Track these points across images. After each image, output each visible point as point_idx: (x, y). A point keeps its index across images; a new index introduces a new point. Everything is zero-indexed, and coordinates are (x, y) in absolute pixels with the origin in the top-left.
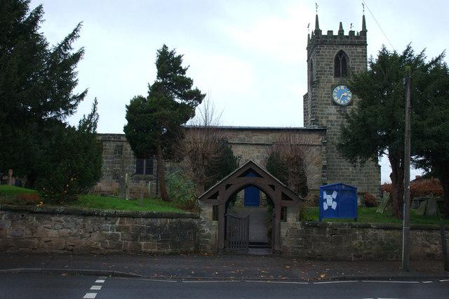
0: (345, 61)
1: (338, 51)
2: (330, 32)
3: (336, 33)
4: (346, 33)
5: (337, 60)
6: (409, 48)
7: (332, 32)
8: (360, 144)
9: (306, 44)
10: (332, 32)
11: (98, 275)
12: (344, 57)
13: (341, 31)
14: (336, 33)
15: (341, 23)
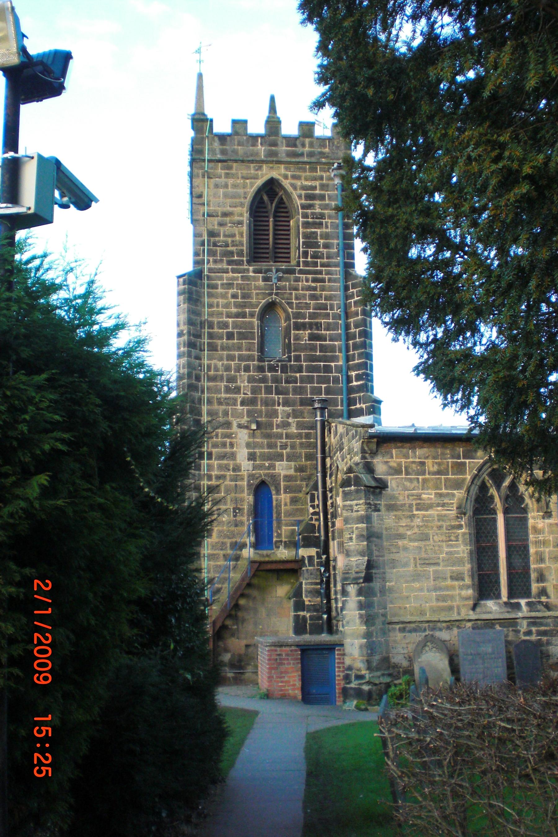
0: (283, 210)
1: (259, 182)
2: (239, 125)
3: (256, 127)
4: (289, 128)
5: (257, 208)
6: (144, 340)
7: (244, 123)
8: (320, 15)
9: (62, 162)
10: (244, 123)
11: (449, 45)
12: (281, 201)
13: (273, 124)
14: (256, 127)
15: (272, 99)
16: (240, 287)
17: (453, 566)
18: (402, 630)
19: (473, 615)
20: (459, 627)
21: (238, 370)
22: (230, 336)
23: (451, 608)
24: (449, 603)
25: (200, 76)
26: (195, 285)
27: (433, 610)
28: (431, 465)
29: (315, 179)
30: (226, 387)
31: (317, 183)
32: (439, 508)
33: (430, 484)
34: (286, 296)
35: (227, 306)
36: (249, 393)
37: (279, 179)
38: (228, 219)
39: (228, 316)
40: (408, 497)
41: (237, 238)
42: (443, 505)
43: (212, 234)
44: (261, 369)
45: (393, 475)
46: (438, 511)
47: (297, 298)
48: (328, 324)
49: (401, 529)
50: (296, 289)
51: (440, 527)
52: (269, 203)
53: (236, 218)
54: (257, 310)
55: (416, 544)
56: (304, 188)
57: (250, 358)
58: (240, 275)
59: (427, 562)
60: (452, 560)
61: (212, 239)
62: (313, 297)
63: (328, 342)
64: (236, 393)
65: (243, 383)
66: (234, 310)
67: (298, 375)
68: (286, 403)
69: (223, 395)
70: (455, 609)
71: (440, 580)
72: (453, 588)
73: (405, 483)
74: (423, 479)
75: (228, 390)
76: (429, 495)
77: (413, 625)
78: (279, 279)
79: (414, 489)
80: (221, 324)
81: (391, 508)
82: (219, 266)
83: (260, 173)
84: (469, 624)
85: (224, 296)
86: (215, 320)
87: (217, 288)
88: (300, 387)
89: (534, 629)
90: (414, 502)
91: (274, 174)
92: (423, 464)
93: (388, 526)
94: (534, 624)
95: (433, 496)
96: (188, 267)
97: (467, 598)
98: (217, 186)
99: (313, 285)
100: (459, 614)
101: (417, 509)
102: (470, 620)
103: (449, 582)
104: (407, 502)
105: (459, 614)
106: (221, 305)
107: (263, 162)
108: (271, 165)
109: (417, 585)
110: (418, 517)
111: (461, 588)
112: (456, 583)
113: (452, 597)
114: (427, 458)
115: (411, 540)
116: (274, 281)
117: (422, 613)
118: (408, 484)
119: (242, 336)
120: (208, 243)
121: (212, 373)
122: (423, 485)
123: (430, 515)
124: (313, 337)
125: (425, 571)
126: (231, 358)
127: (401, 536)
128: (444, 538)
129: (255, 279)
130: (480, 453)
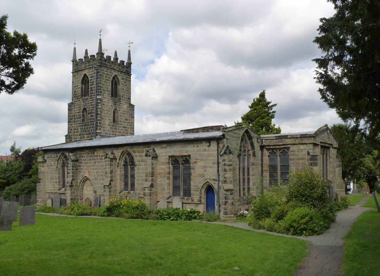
15: (86, 50)
23: (55, 190)
28: (53, 156)
33: (53, 160)
39: (77, 113)
43: (75, 92)
66: (78, 111)
76: (52, 163)
92: (52, 156)
126: (77, 124)
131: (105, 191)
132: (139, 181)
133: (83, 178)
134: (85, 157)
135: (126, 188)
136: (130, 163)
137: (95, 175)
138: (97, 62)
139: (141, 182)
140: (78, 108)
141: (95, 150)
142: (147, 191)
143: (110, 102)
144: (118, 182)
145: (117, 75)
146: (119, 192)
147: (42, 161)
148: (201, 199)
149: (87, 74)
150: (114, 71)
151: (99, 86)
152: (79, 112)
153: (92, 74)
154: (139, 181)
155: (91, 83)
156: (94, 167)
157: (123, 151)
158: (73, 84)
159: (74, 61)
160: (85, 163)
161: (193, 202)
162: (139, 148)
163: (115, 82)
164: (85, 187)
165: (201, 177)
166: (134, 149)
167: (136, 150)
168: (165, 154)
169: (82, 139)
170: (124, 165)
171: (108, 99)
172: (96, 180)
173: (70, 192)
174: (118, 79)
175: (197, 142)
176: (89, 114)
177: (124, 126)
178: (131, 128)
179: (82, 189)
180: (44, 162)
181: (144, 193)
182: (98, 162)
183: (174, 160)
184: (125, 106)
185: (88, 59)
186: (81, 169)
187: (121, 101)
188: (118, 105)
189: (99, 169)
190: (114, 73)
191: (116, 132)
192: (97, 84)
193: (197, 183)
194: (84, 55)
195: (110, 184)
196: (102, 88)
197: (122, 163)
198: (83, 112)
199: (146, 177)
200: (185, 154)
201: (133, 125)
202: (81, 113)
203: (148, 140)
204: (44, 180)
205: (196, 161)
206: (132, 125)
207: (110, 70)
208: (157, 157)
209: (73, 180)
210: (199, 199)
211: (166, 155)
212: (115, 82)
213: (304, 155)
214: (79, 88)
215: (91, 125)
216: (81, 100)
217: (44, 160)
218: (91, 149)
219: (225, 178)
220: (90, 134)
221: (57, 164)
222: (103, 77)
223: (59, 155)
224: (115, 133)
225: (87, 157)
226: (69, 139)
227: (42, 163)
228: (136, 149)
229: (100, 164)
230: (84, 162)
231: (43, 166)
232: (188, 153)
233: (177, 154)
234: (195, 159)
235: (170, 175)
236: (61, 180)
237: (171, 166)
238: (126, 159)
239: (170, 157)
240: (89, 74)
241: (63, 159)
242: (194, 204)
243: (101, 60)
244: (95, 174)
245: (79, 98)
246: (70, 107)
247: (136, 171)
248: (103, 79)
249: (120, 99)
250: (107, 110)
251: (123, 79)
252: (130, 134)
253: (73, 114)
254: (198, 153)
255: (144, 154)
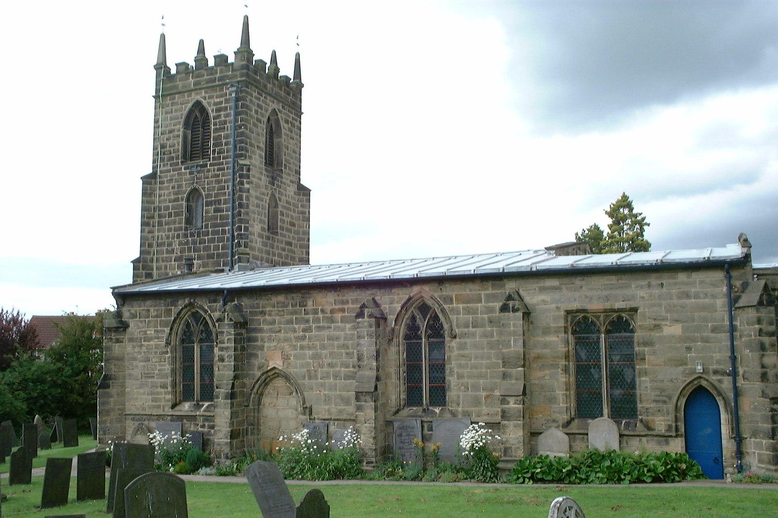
1: (190, 105)
13: (245, 50)
15: (202, 43)
16: (176, 181)
17: (162, 379)
18: (133, 419)
19: (171, 412)
20: (163, 420)
21: (173, 238)
22: (170, 215)
23: (159, 407)
24: (158, 403)
25: (163, 37)
26: (150, 183)
27: (150, 407)
28: (153, 312)
29: (221, 96)
30: (167, 249)
31: (223, 99)
32: (156, 340)
33: (152, 324)
34: (202, 183)
35: (169, 194)
36: (179, 253)
37: (201, 101)
38: (171, 135)
39: (170, 202)
40: (140, 333)
41: (176, 147)
42: (158, 338)
43: (163, 147)
44: (186, 236)
45: (132, 318)
46: (155, 342)
47: (208, 184)
48: (225, 199)
49: (135, 354)
50: (208, 178)
51: (156, 353)
52: (197, 120)
53: (176, 133)
54: (185, 195)
55: (142, 364)
56: (215, 104)
57: (180, 229)
58: (176, 172)
59: (148, 375)
60: (162, 375)
61: (163, 150)
62: (218, 182)
63: (225, 213)
64: (172, 254)
65: (176, 246)
66: (172, 197)
67: (206, 238)
68: (199, 258)
69: (165, 255)
70: (162, 408)
71: (154, 388)
72: (161, 393)
73: (139, 324)
74: (149, 321)
75: (168, 252)
76: (151, 332)
77: (139, 417)
78: (198, 172)
79: (143, 328)
80: (166, 208)
81: (131, 340)
82: (166, 168)
83: (190, 98)
84: (169, 418)
85: (167, 188)
86: (163, 205)
87: (164, 183)
88: (207, 246)
89: (206, 424)
90: (143, 337)
91: (198, 98)
92: (148, 311)
93: (128, 352)
94: (207, 420)
95: (153, 332)
96: (149, 170)
97: (168, 401)
98: (167, 113)
99: (218, 173)
100: (163, 411)
101: (144, 341)
102: (168, 415)
103: (159, 390)
104: (139, 336)
105: (163, 411)
106: (164, 195)
107: (192, 90)
108: (196, 92)
109: (142, 391)
110: (144, 346)
111: (165, 393)
112: (163, 390)
113: (160, 400)
114: (151, 306)
115: (140, 361)
116: (195, 173)
117: (144, 409)
118: (140, 324)
119: (177, 214)
120: (160, 152)
121: (160, 241)
122: (148, 325)
123: (150, 344)
124: (216, 211)
125: (146, 381)
126: (170, 230)
127: (135, 359)
128: (158, 360)
129: (185, 174)
130: (180, 302)
131: (359, 408)
132: (465, 380)
133: (263, 374)
134: (270, 315)
135: (413, 397)
136: (430, 332)
137: (308, 364)
138: (238, 73)
139: (470, 381)
140: (173, 188)
141: (307, 295)
142: (513, 405)
143: (263, 177)
144: (394, 379)
145: (277, 110)
146: (394, 410)
147: (115, 325)
148: (679, 424)
149: (205, 103)
150: (272, 99)
151: (242, 134)
152: (176, 200)
153: (221, 103)
154: (465, 380)
155: (215, 124)
156: (305, 343)
157: (410, 299)
158: (156, 128)
159: (161, 67)
160: (272, 331)
161: (650, 433)
162: (465, 291)
163: (273, 132)
164: (266, 400)
165: (676, 366)
166: (446, 291)
167: (664, 282)
168: (554, 306)
169: (189, 271)
170: (407, 337)
171: (260, 168)
172: (310, 378)
173: (228, 412)
174: (277, 121)
175: (658, 275)
176: (207, 205)
177: (287, 239)
178: (301, 247)
179: (256, 403)
180: (120, 328)
181: (503, 412)
182: (318, 327)
183: (581, 325)
184: (292, 190)
185: (201, 68)
186: (254, 348)
187: (284, 176)
188: (278, 185)
189: (323, 347)
190: (271, 104)
191: (274, 255)
192: (236, 129)
193: (658, 381)
194: (237, 44)
195: (376, 388)
196: (248, 140)
197: (402, 330)
198: (188, 200)
199: (503, 367)
200: (618, 305)
201: (306, 239)
202: (184, 203)
203: (497, 266)
204: (120, 381)
205: (657, 323)
206: (304, 240)
207: (264, 95)
208: (530, 313)
209: (236, 377)
210: (670, 423)
211: (557, 308)
212: (273, 132)
213: (270, 339)
214: (178, 136)
215: (214, 233)
216: (183, 167)
217: (121, 322)
218: (292, 292)
219: (763, 367)
220: (211, 256)
221: (170, 334)
222: (251, 111)
223: (175, 310)
224: (271, 257)
225: (277, 315)
226: (143, 269)
227: (115, 331)
228: (451, 290)
229: (326, 333)
230: (266, 327)
231: (118, 341)
232: (630, 303)
233: (415, 318)
234: (655, 319)
235: (569, 361)
236: (178, 378)
237: (571, 338)
238: (413, 318)
239: (568, 312)
240: (209, 103)
241: (187, 320)
242: (656, 438)
243: (247, 67)
244: (247, 362)
245: (177, 164)
246: (149, 186)
247: (456, 352)
248: (251, 116)
249: (282, 170)
250: (257, 198)
251: (287, 122)
252: (299, 261)
253: (157, 204)
254: (663, 302)
255: (498, 305)
